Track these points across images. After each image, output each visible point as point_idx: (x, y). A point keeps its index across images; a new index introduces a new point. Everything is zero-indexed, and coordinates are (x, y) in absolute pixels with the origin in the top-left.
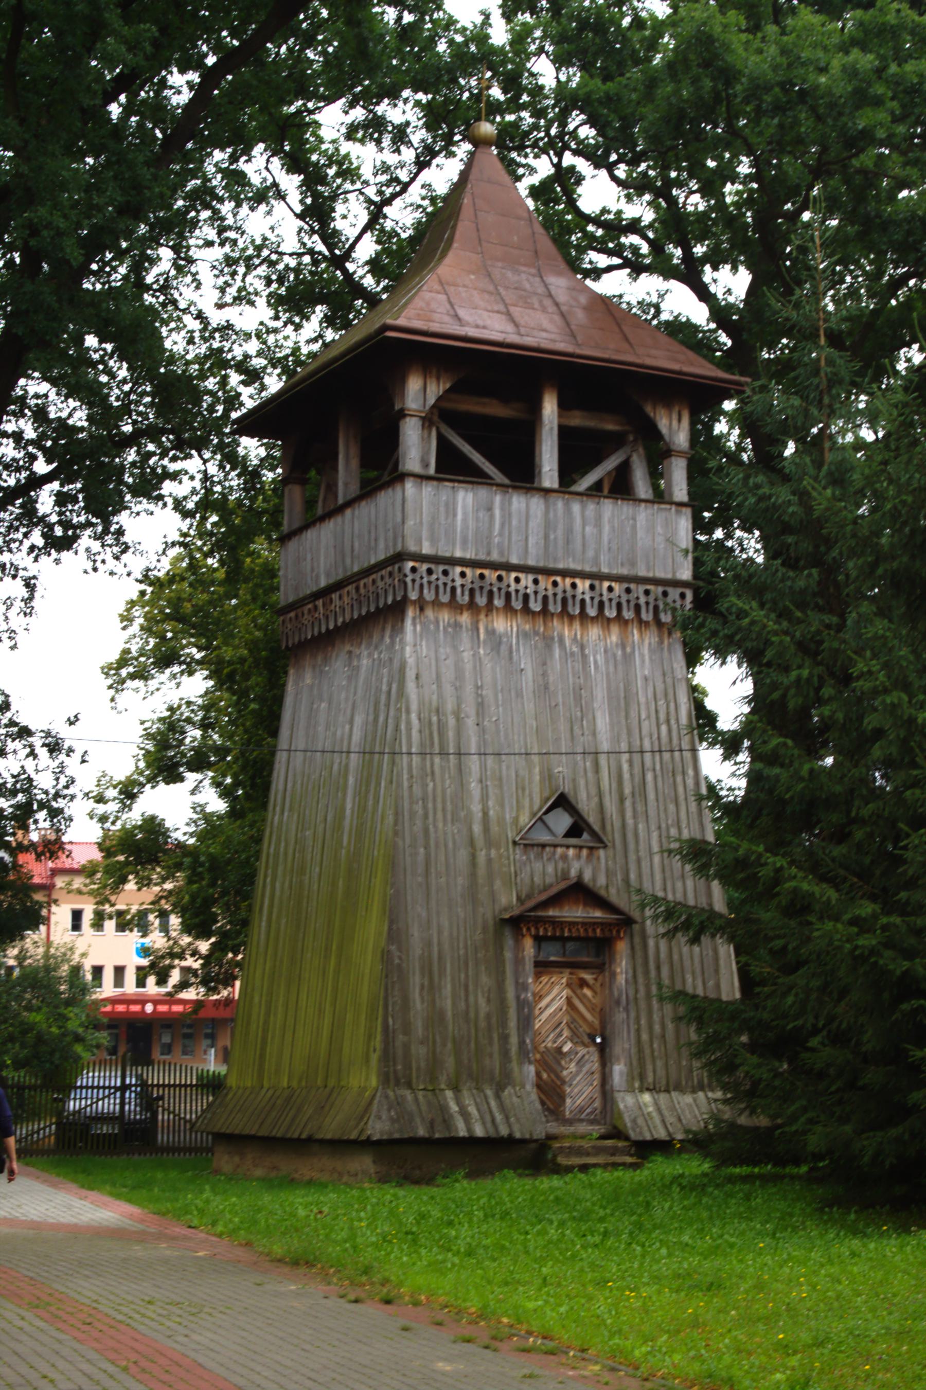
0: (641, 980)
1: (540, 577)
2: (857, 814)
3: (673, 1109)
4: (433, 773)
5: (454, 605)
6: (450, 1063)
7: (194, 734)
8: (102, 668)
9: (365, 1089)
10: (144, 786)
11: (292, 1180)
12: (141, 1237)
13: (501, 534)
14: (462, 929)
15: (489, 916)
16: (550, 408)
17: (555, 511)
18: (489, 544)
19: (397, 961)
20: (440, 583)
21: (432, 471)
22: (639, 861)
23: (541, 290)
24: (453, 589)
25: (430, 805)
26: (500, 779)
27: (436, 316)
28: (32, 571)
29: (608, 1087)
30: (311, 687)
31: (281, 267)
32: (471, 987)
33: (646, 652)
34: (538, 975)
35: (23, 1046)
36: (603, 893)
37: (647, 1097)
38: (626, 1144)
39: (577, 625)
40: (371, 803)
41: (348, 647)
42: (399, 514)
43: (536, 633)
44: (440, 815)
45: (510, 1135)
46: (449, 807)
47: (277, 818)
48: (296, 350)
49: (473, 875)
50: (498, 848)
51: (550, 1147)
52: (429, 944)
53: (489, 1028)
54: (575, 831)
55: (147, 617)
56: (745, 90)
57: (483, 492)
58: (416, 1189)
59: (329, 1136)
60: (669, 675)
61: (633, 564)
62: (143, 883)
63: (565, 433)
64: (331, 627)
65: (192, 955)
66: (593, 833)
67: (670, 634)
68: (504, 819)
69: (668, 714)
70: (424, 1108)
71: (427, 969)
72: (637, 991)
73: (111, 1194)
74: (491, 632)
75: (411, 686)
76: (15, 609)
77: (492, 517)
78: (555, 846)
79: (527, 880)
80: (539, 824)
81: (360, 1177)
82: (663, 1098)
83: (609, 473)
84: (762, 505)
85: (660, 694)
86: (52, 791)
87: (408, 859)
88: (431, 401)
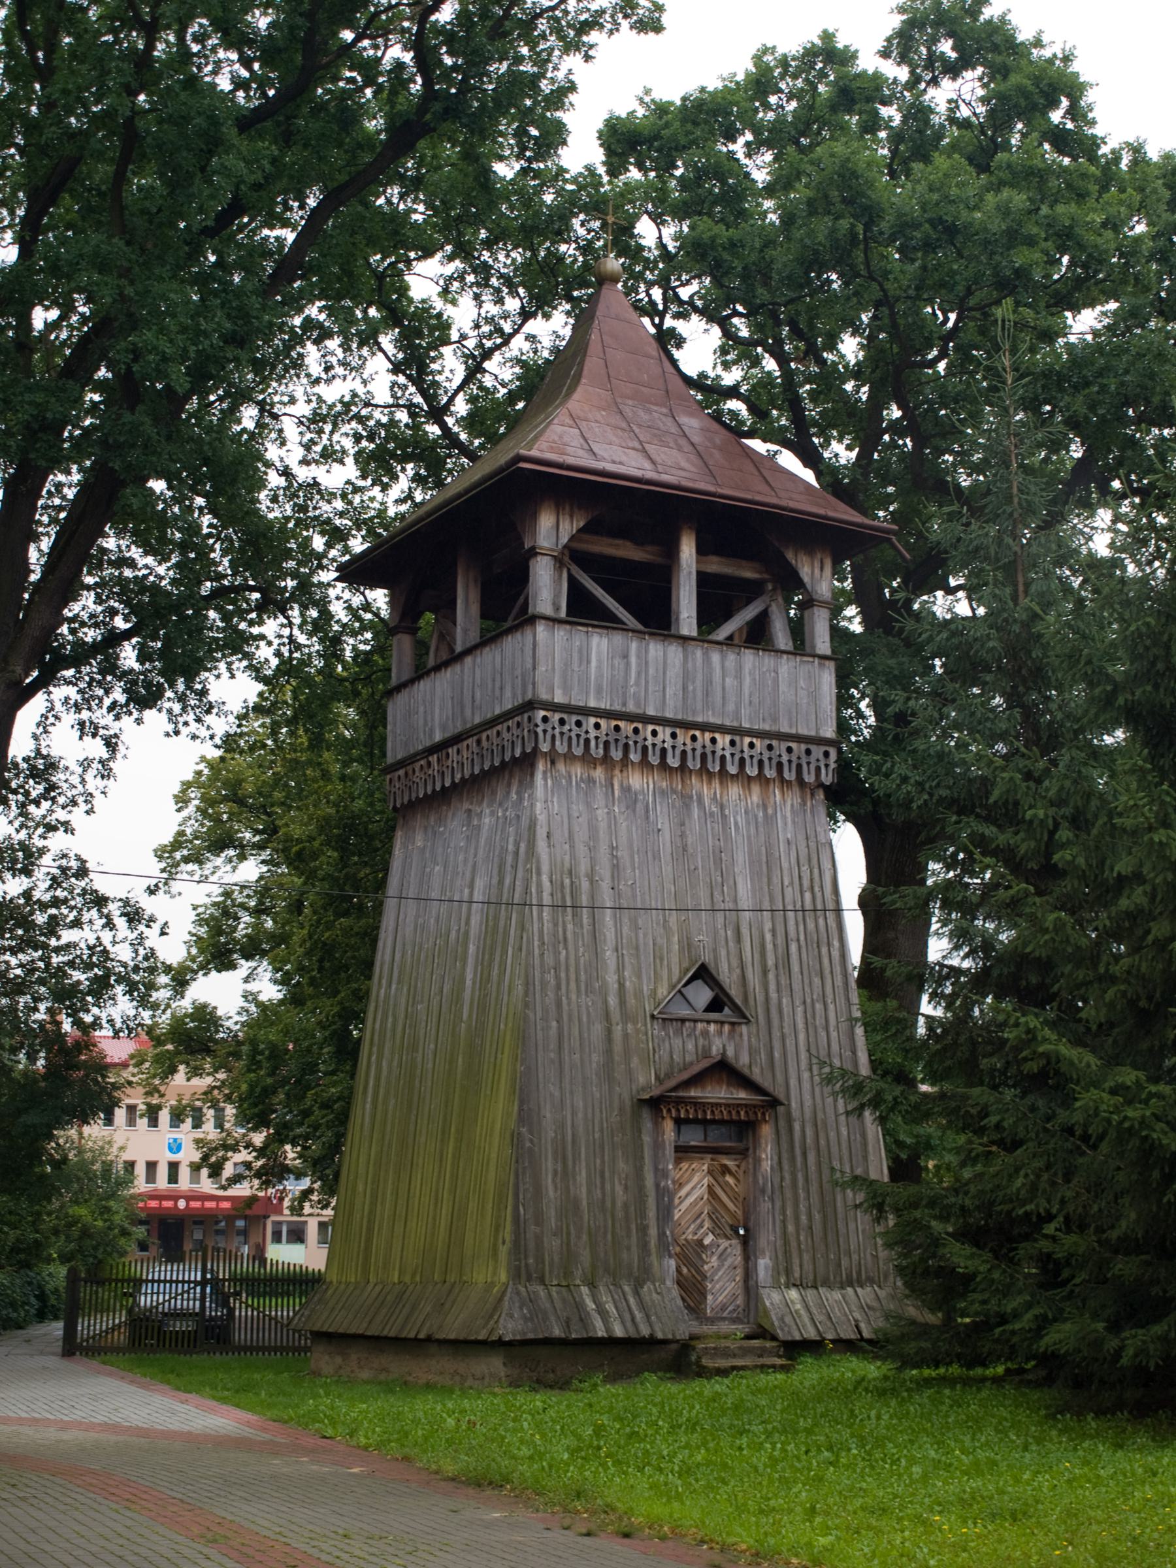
0: (786, 1167)
1: (678, 731)
2: (1107, 970)
3: (821, 1305)
4: (565, 939)
5: (587, 759)
6: (585, 1256)
7: (245, 922)
8: (155, 851)
9: (493, 1284)
10: (196, 972)
11: (405, 1383)
12: (273, 1449)
13: (637, 684)
15: (626, 1096)
16: (688, 550)
17: (694, 660)
18: (624, 694)
19: (528, 1144)
20: (573, 734)
21: (563, 614)
22: (783, 1038)
23: (674, 430)
24: (587, 741)
25: (563, 975)
26: (637, 948)
27: (570, 450)
28: (115, 727)
29: (751, 1283)
30: (423, 850)
31: (372, 423)
32: (607, 1174)
33: (788, 814)
34: (678, 1161)
35: (68, 1239)
36: (746, 1071)
37: (793, 1294)
38: (775, 1344)
39: (716, 783)
40: (495, 972)
41: (466, 806)
42: (529, 660)
43: (674, 791)
44: (573, 985)
45: (651, 1335)
46: (583, 977)
47: (383, 991)
48: (382, 513)
49: (609, 1052)
50: (635, 1023)
51: (694, 1348)
52: (562, 1126)
53: (627, 1218)
54: (715, 1006)
55: (203, 799)
56: (891, 227)
57: (618, 638)
58: (549, 1392)
59: (452, 1336)
60: (812, 838)
61: (775, 719)
62: (195, 1072)
63: (704, 580)
64: (447, 784)
65: (246, 1147)
66: (736, 1008)
67: (812, 795)
68: (641, 991)
69: (812, 880)
70: (559, 1305)
71: (560, 1154)
72: (782, 1179)
73: (214, 1398)
74: (626, 789)
75: (541, 845)
76: (91, 773)
77: (628, 664)
78: (695, 1021)
79: (666, 1058)
80: (679, 996)
81: (487, 1380)
82: (810, 1294)
83: (740, 629)
84: (955, 641)
85: (803, 860)
86: (132, 964)
87: (540, 1034)
88: (564, 540)
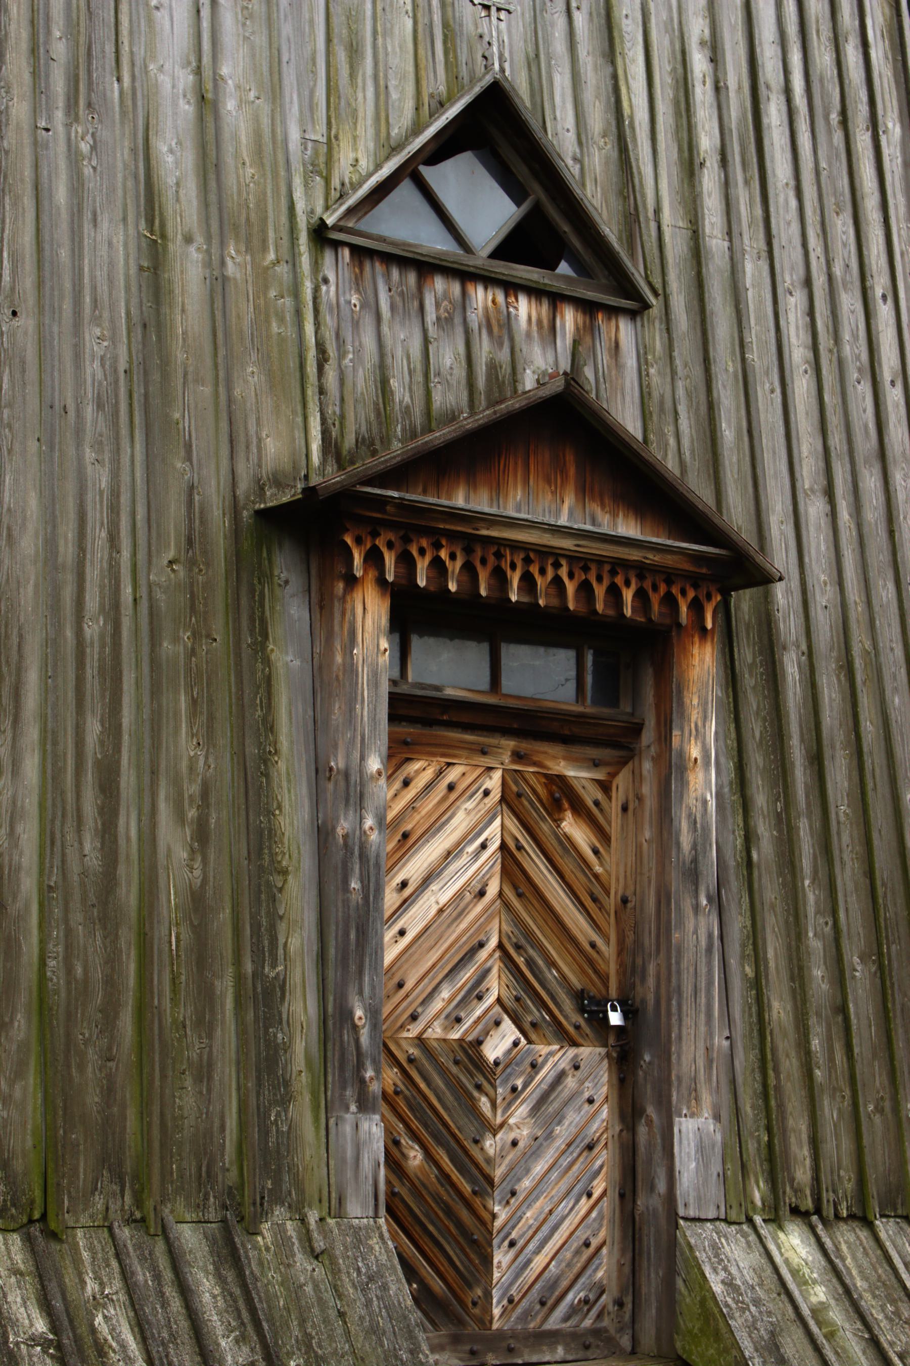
14: (99, 536)
32: (128, 780)
72: (749, 838)
80: (406, 191)
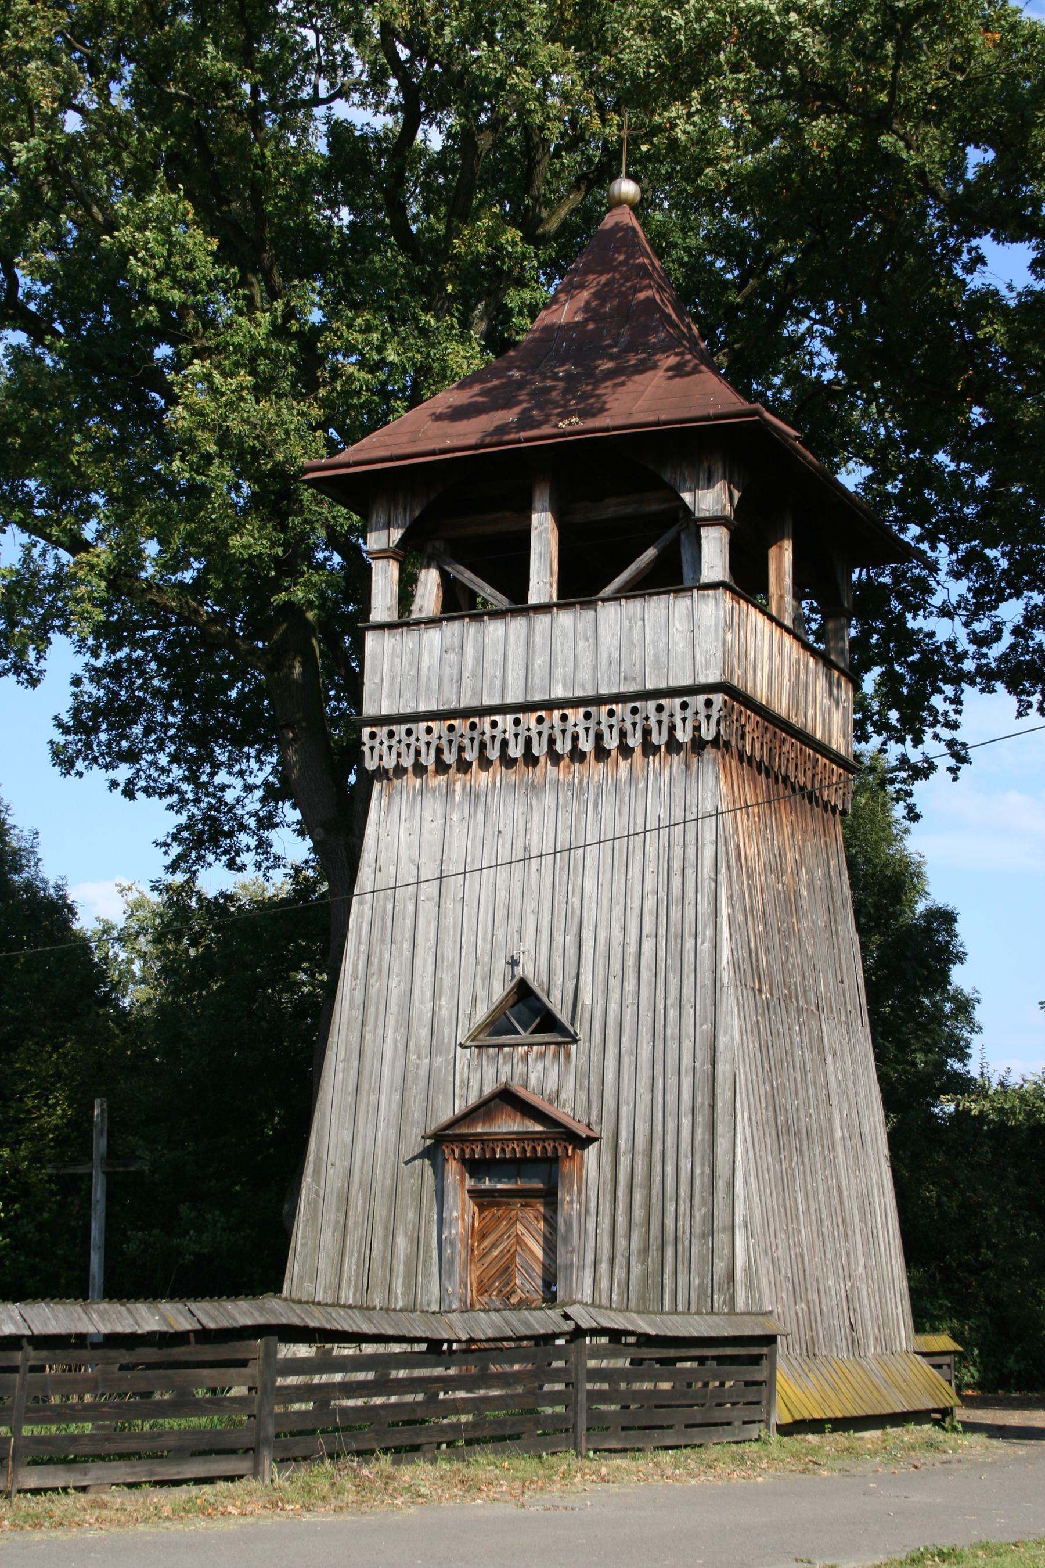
3: (15, 1323)
